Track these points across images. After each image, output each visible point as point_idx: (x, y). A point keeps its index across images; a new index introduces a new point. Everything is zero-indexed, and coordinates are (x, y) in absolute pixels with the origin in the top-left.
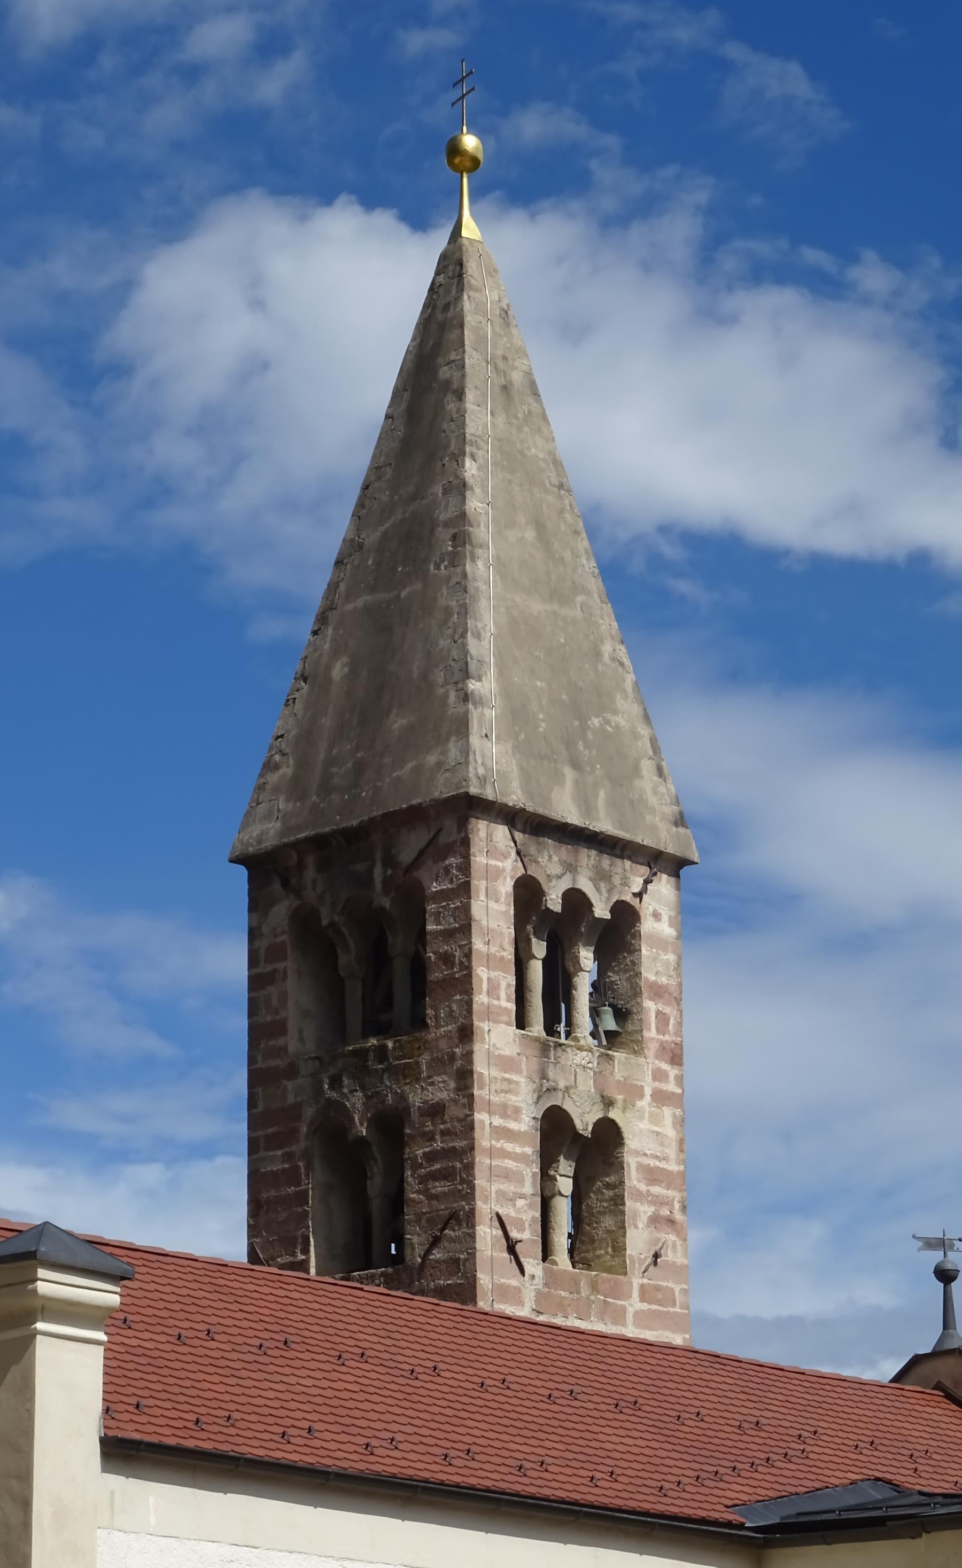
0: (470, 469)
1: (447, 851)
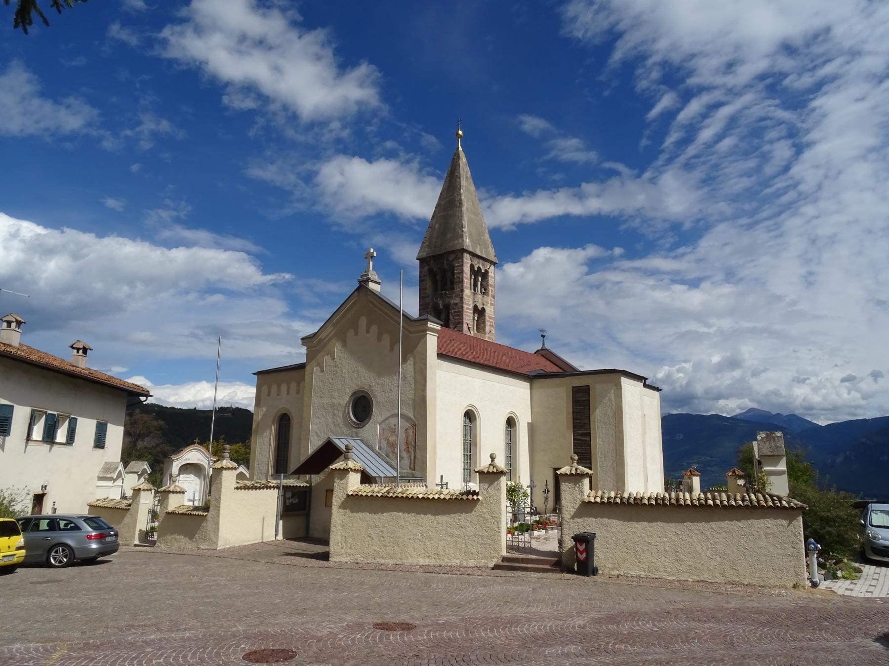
0: (462, 191)
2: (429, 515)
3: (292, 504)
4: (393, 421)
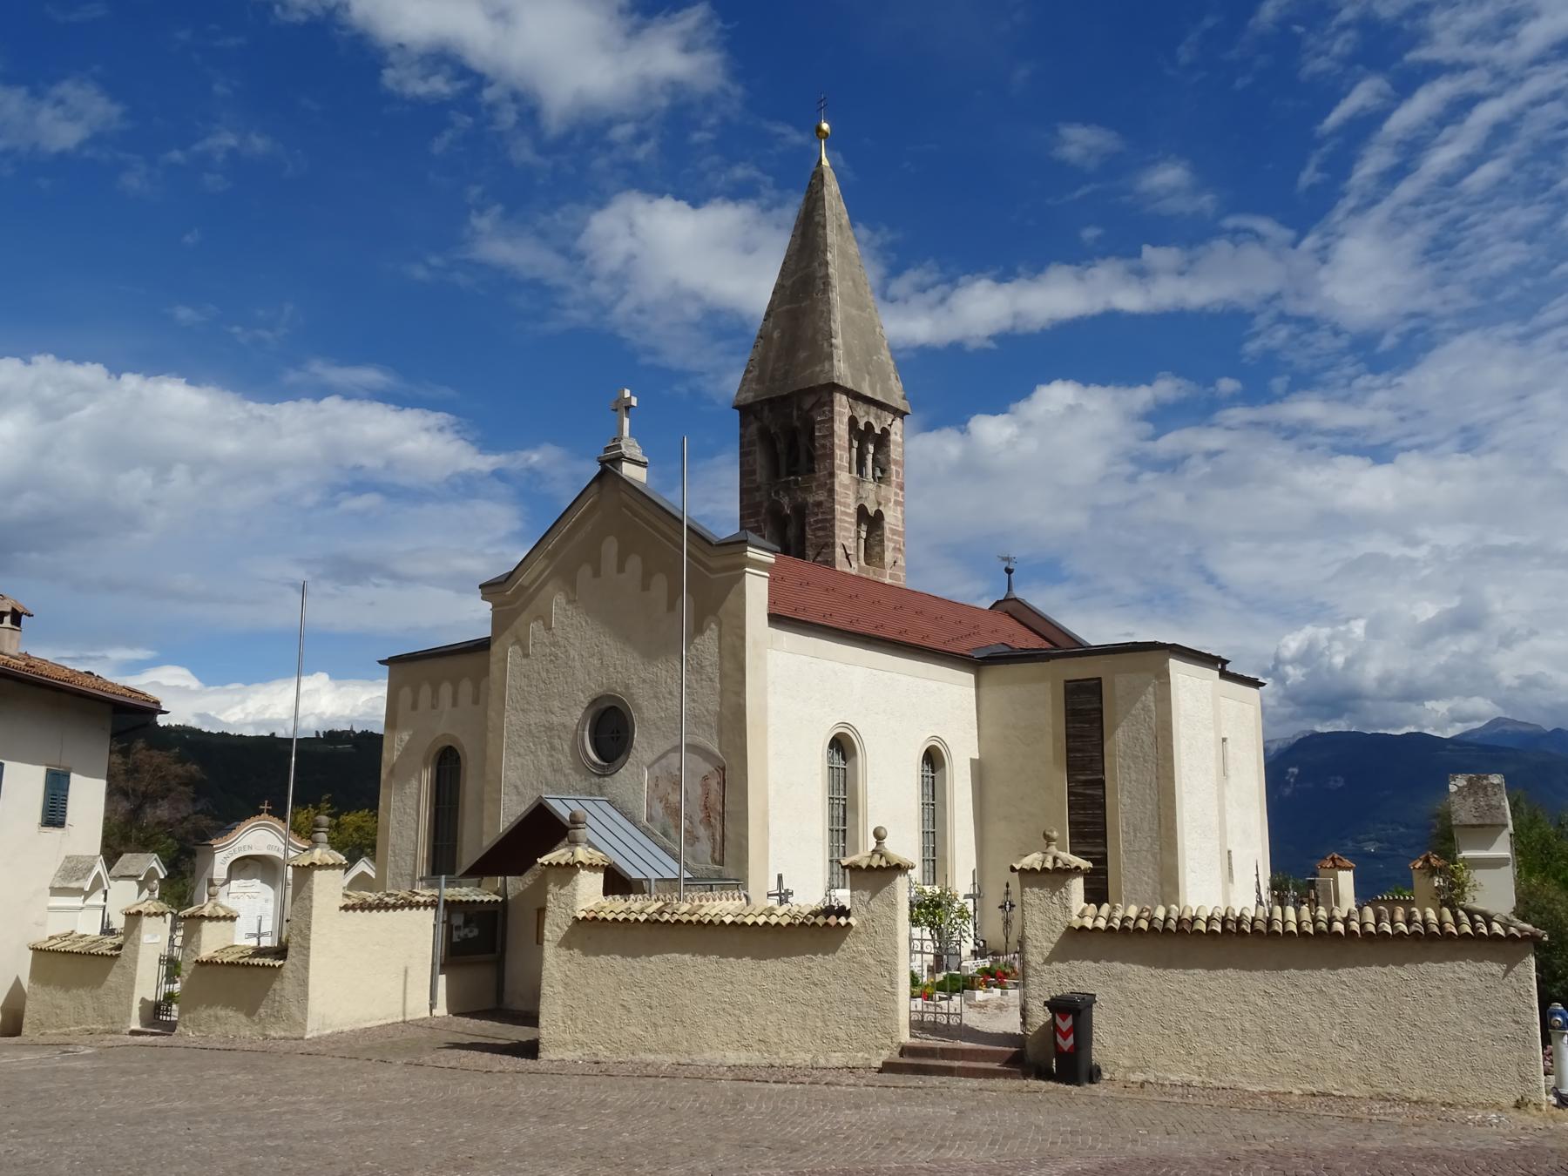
1: (824, 405)
2: (747, 960)
3: (465, 940)
4: (674, 757)
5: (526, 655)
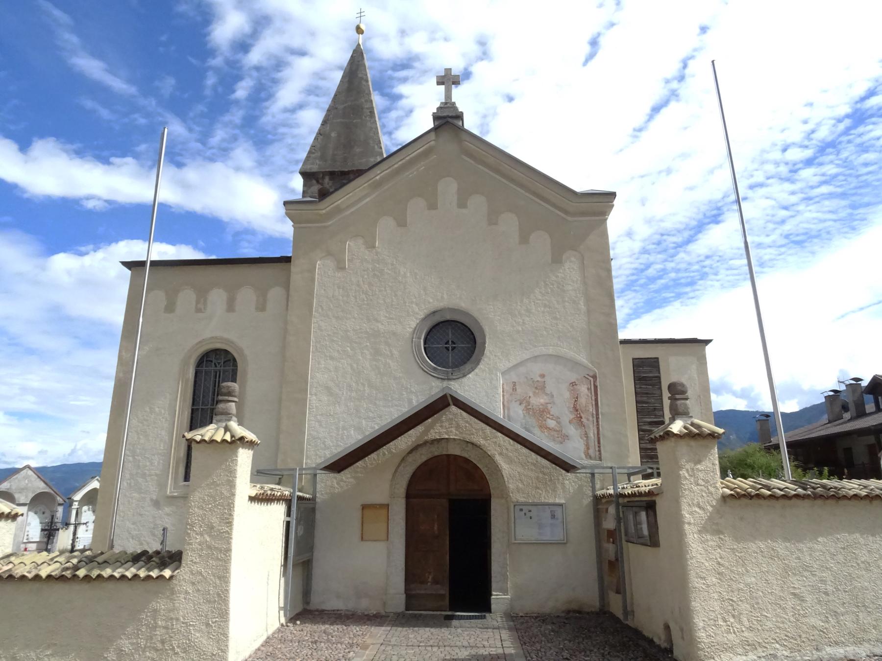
5: (343, 268)
